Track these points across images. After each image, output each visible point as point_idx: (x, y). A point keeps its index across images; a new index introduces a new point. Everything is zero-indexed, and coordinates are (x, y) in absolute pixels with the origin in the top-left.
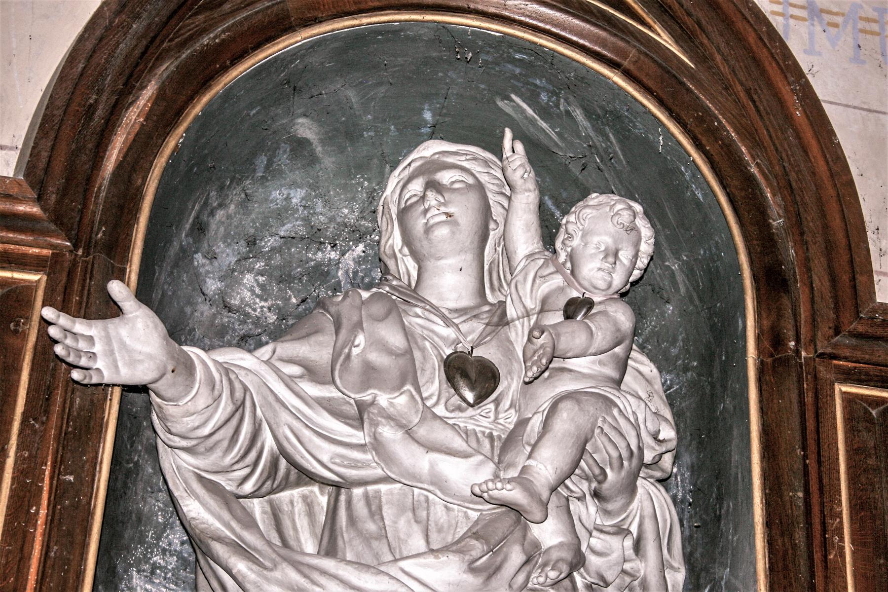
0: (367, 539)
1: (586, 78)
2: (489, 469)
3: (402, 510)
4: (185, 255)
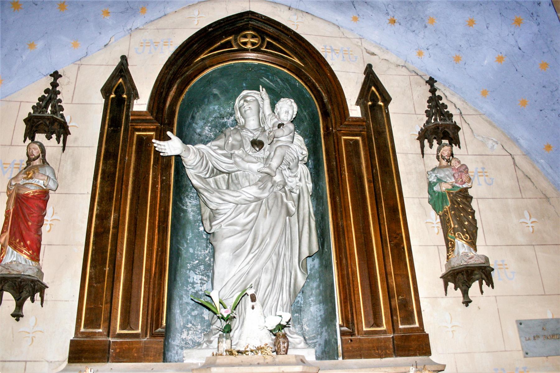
0: (236, 185)
1: (279, 72)
2: (262, 165)
3: (243, 177)
4: (190, 124)
